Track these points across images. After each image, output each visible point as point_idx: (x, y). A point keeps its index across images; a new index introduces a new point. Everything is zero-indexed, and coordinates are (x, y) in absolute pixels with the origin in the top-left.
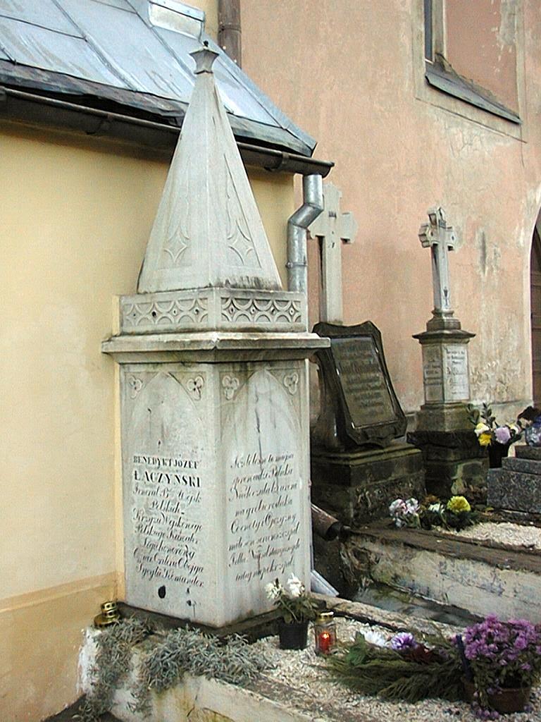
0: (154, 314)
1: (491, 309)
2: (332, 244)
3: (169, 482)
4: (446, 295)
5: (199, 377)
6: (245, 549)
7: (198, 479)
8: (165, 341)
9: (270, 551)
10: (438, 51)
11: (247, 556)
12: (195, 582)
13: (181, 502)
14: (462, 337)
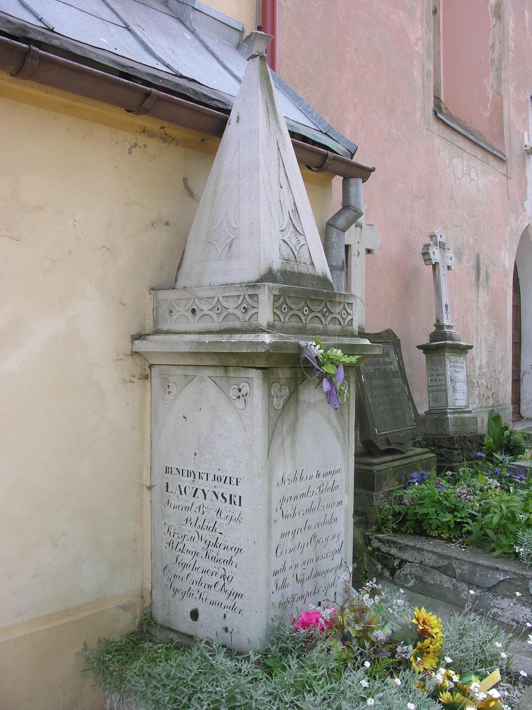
0: (194, 311)
1: (480, 321)
2: (357, 253)
3: (205, 498)
4: (447, 310)
5: (245, 384)
6: (289, 573)
7: (240, 497)
8: (207, 341)
9: (314, 573)
10: (437, 95)
11: (291, 580)
12: (233, 608)
13: (219, 521)
14: (462, 350)
